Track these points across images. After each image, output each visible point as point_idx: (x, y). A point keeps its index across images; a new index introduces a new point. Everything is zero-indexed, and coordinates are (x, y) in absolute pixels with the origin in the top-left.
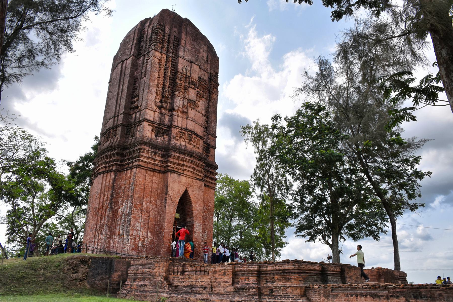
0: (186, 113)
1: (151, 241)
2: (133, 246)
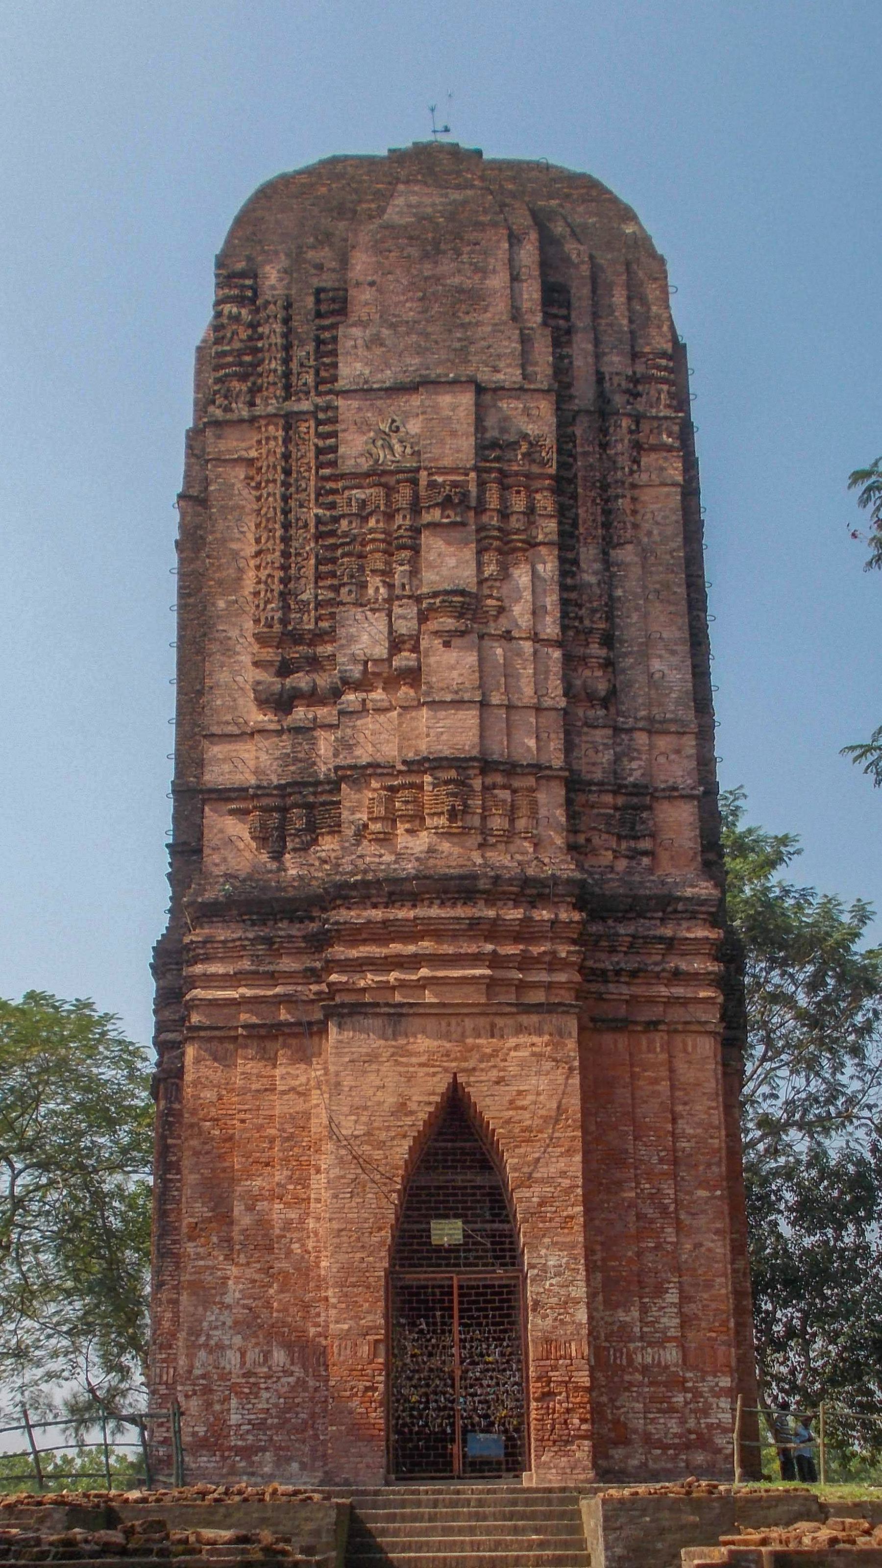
0: (413, 676)
1: (292, 1388)
2: (201, 1430)
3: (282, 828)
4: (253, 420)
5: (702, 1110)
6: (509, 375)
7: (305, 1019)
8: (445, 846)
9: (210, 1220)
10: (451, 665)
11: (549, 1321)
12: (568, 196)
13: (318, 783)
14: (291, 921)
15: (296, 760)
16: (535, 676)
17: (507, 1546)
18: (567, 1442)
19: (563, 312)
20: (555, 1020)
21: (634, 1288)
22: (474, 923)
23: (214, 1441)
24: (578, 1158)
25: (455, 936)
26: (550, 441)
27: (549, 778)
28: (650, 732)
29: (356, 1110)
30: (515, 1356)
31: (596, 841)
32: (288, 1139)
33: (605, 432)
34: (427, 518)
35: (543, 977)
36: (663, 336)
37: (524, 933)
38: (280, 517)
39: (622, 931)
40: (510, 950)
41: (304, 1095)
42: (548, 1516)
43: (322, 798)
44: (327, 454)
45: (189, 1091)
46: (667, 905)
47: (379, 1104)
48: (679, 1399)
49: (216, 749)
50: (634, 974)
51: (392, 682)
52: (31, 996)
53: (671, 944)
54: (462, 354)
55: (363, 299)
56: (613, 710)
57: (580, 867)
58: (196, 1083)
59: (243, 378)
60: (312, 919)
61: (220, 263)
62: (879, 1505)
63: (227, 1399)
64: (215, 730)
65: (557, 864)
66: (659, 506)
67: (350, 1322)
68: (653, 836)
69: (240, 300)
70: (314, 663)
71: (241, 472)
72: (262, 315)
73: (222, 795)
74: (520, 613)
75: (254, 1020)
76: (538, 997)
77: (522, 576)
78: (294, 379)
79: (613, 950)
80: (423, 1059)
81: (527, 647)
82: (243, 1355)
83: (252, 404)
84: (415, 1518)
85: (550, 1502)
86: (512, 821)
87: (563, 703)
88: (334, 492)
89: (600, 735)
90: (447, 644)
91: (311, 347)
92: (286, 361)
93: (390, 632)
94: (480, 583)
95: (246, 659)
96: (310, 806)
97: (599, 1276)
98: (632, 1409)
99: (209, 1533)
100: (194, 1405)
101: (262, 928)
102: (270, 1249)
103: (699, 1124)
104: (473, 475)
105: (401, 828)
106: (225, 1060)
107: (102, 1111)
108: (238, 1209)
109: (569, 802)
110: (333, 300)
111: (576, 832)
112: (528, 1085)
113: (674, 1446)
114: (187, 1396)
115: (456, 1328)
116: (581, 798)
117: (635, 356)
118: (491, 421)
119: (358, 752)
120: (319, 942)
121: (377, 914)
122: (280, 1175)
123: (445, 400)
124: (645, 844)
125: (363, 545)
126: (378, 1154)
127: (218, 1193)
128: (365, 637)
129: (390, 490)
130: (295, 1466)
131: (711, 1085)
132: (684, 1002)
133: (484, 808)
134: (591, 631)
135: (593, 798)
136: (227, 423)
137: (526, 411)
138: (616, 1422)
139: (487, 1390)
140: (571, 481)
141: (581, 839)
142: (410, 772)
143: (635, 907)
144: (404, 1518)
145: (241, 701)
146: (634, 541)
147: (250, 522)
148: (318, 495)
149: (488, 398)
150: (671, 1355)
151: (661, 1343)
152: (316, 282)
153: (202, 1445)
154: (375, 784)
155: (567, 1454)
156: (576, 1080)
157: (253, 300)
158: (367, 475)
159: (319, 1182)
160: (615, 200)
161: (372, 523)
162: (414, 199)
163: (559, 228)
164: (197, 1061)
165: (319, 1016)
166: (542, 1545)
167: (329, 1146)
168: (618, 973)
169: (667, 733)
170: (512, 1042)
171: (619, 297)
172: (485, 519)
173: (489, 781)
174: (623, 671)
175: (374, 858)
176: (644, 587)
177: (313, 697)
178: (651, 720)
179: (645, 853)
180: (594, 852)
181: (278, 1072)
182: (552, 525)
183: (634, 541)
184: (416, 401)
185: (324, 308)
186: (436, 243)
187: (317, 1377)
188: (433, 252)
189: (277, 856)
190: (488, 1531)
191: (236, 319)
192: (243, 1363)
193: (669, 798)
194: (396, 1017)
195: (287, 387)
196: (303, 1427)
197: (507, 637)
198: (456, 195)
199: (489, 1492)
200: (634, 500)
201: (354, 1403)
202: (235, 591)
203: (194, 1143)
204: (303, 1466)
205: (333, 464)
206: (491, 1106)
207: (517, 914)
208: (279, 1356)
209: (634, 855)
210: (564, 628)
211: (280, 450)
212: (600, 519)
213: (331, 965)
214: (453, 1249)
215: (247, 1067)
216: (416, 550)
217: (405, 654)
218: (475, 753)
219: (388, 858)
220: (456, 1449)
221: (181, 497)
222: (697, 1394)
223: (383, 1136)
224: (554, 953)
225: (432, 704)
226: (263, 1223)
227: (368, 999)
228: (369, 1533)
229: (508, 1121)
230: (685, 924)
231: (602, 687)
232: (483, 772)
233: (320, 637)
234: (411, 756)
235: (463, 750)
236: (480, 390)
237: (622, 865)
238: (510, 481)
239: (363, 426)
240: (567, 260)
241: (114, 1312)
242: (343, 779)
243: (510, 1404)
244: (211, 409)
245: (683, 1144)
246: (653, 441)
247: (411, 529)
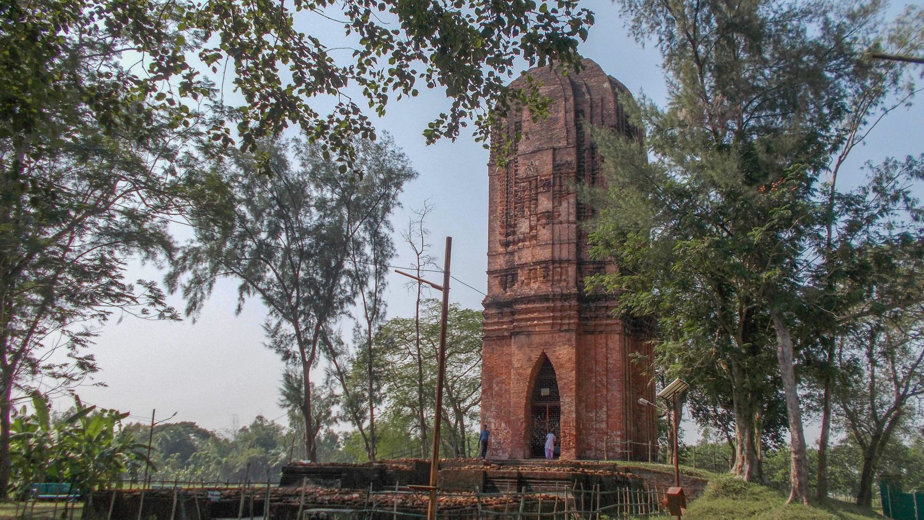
0: (535, 237)
10: (544, 234)
22: (548, 308)
34: (539, 190)
50: (596, 317)
62: (2, 499)
74: (563, 218)
76: (566, 327)
77: (565, 204)
98: (592, 440)
112: (563, 354)
118: (558, 158)
120: (513, 313)
128: (524, 226)
129: (530, 182)
132: (611, 325)
150: (604, 425)
175: (527, 291)
189: (505, 289)
198: (552, 88)
208: (503, 425)
239: (524, 165)
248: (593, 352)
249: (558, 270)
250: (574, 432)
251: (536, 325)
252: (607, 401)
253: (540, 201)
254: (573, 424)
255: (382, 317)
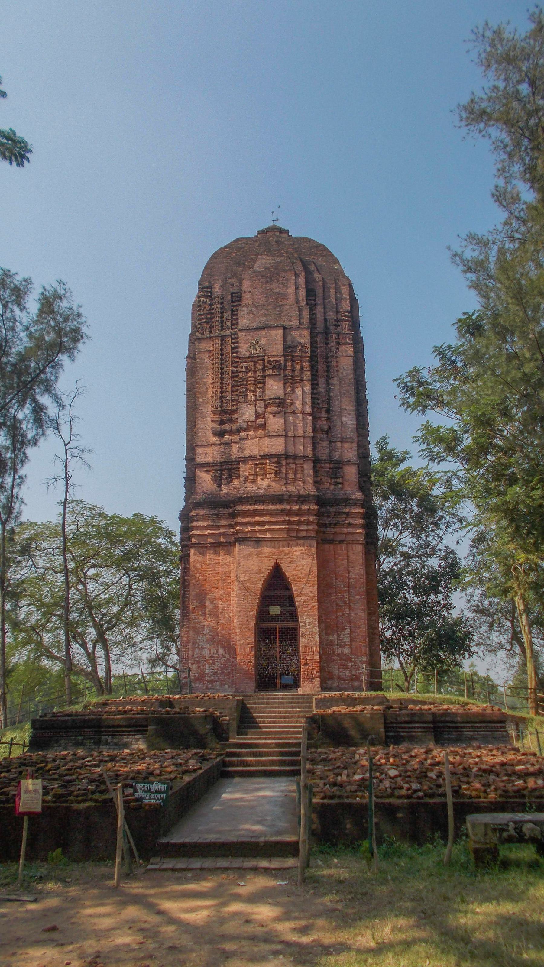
0: (263, 427)
1: (226, 661)
3: (221, 476)
4: (211, 338)
5: (358, 571)
6: (295, 323)
7: (229, 541)
8: (274, 484)
9: (199, 607)
10: (276, 423)
11: (306, 640)
12: (316, 254)
13: (232, 462)
14: (224, 508)
15: (225, 454)
16: (303, 426)
17: (289, 712)
18: (312, 679)
19: (313, 298)
20: (309, 541)
21: (335, 629)
22: (283, 510)
23: (201, 678)
24: (316, 587)
25: (277, 514)
26: (308, 345)
27: (308, 460)
28: (341, 442)
29: (245, 572)
30: (297, 650)
31: (324, 480)
32: (223, 580)
33: (327, 339)
34: (268, 373)
35: (305, 527)
36: (347, 305)
37: (299, 513)
38: (220, 371)
39: (331, 510)
40: (295, 519)
41: (229, 566)
42: (302, 703)
43: (234, 467)
44: (235, 349)
45: (192, 564)
46: (347, 501)
47: (252, 570)
48: (350, 664)
49: (200, 450)
50: (335, 525)
51: (257, 428)
52: (136, 515)
53: (348, 514)
54: (279, 316)
55: (246, 296)
56: (330, 435)
57: (318, 489)
58: (194, 562)
59: (207, 323)
60: (231, 508)
61: (200, 284)
63: (204, 665)
64: (199, 443)
65: (310, 489)
66: (345, 363)
67: (244, 641)
68: (342, 477)
69: (206, 296)
70: (231, 421)
71: (207, 355)
72: (214, 301)
73: (202, 466)
74: (298, 403)
75: (213, 541)
76: (303, 534)
78: (224, 324)
79: (329, 517)
80: (267, 555)
81: (300, 416)
82: (210, 651)
83: (211, 332)
84: (262, 703)
85: (304, 698)
86: (296, 475)
87: (312, 435)
88: (237, 362)
89: (325, 444)
90: (274, 416)
91: (229, 313)
92: (222, 317)
93: (256, 412)
94: (285, 394)
95: (209, 419)
96: (230, 469)
97: (324, 624)
98: (335, 668)
99: (198, 709)
100: (194, 667)
101: (216, 510)
102: (218, 616)
103: (357, 574)
104: (283, 358)
105: (259, 478)
106: (203, 554)
107: (160, 554)
108: (208, 603)
109: (314, 467)
110: (237, 297)
111: (317, 477)
112: (300, 563)
113: (347, 680)
114: (192, 664)
115: (278, 642)
116: (318, 465)
117: (337, 312)
118: (289, 338)
119: (245, 452)
120: (233, 515)
121: (251, 507)
122: (221, 592)
123: (273, 332)
124: (340, 480)
125: (247, 382)
126: (252, 586)
127: (202, 597)
128: (247, 413)
129: (255, 363)
130: (227, 686)
131: (361, 561)
133: (286, 471)
134: (322, 408)
135: (323, 465)
136: (202, 338)
137: (301, 335)
138: (329, 672)
139: (287, 662)
140: (316, 357)
141: (319, 479)
142: (262, 459)
143: (336, 502)
144: (259, 704)
145: (207, 433)
146: (337, 376)
147: (210, 372)
148: (232, 363)
149: (288, 331)
150: (347, 650)
151: (344, 646)
152: (231, 290)
153: (197, 679)
154: (250, 463)
155: (312, 683)
156: (315, 562)
157: (210, 296)
158: (248, 358)
159: (233, 594)
160: (332, 255)
161: (250, 374)
162: (263, 261)
163: (312, 268)
164: (194, 554)
165: (233, 540)
166: (300, 712)
167: (236, 583)
168: (330, 524)
169: (347, 442)
170: (295, 549)
171: (332, 292)
172: (287, 372)
173: (288, 461)
174: (333, 421)
175: (251, 488)
176: (340, 392)
177: (231, 432)
178: (342, 438)
179: (340, 483)
180: (323, 483)
181: (221, 558)
182: (309, 374)
183: (337, 376)
184: (264, 332)
185: (234, 299)
186: (271, 277)
187: (234, 658)
188: (270, 280)
189: (219, 486)
190: (284, 708)
191: (205, 303)
192: (210, 653)
193: (348, 464)
194: (258, 542)
195: (222, 326)
196: (228, 675)
197: (294, 413)
198: (278, 259)
199: (285, 695)
200: (337, 362)
201: (245, 667)
202: (205, 396)
203: (193, 581)
204: (229, 686)
205: (237, 352)
206: (288, 570)
207: (297, 507)
208: (221, 651)
209: (337, 484)
210: (313, 408)
211: (220, 348)
212: (325, 369)
213: (237, 524)
214: (277, 616)
215: (210, 556)
216: (264, 383)
217: (261, 419)
218: (283, 452)
219: (255, 488)
220: (278, 681)
221: (187, 357)
222: (355, 663)
223: (254, 580)
224: (309, 519)
225: (269, 437)
226: (216, 607)
227: (249, 535)
228: (248, 708)
229: (293, 575)
230: (353, 507)
231: (326, 428)
232: (286, 459)
233: (233, 412)
234: (262, 453)
235: (279, 452)
236: (285, 328)
237: (332, 487)
238: (295, 359)
239: (246, 341)
240: (314, 280)
241: (163, 626)
242: (241, 461)
243: (295, 666)
244: (197, 333)
245: (351, 581)
246: (343, 341)
247: (262, 376)
248: (332, 564)
249: (293, 466)
250: (317, 659)
251: (267, 531)
252: (350, 622)
253: (268, 386)
254: (316, 649)
255: (16, 518)
